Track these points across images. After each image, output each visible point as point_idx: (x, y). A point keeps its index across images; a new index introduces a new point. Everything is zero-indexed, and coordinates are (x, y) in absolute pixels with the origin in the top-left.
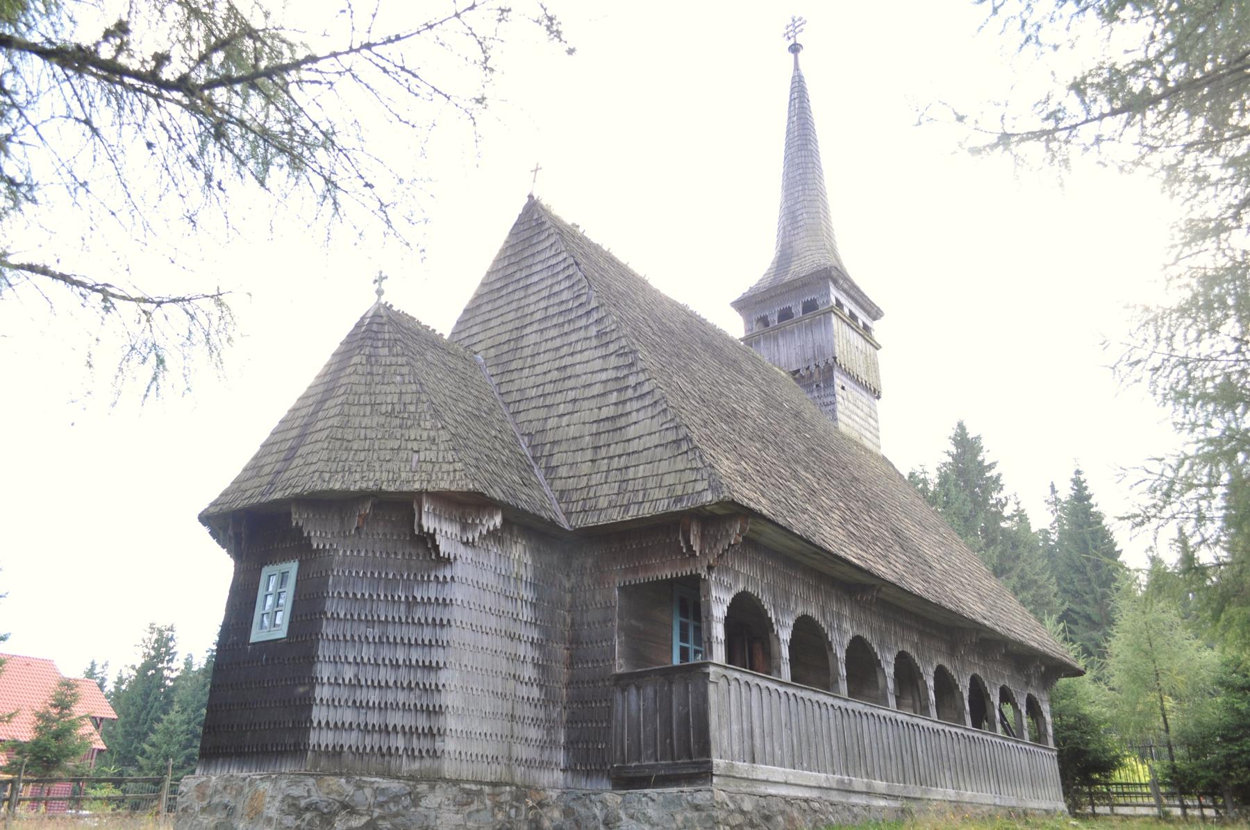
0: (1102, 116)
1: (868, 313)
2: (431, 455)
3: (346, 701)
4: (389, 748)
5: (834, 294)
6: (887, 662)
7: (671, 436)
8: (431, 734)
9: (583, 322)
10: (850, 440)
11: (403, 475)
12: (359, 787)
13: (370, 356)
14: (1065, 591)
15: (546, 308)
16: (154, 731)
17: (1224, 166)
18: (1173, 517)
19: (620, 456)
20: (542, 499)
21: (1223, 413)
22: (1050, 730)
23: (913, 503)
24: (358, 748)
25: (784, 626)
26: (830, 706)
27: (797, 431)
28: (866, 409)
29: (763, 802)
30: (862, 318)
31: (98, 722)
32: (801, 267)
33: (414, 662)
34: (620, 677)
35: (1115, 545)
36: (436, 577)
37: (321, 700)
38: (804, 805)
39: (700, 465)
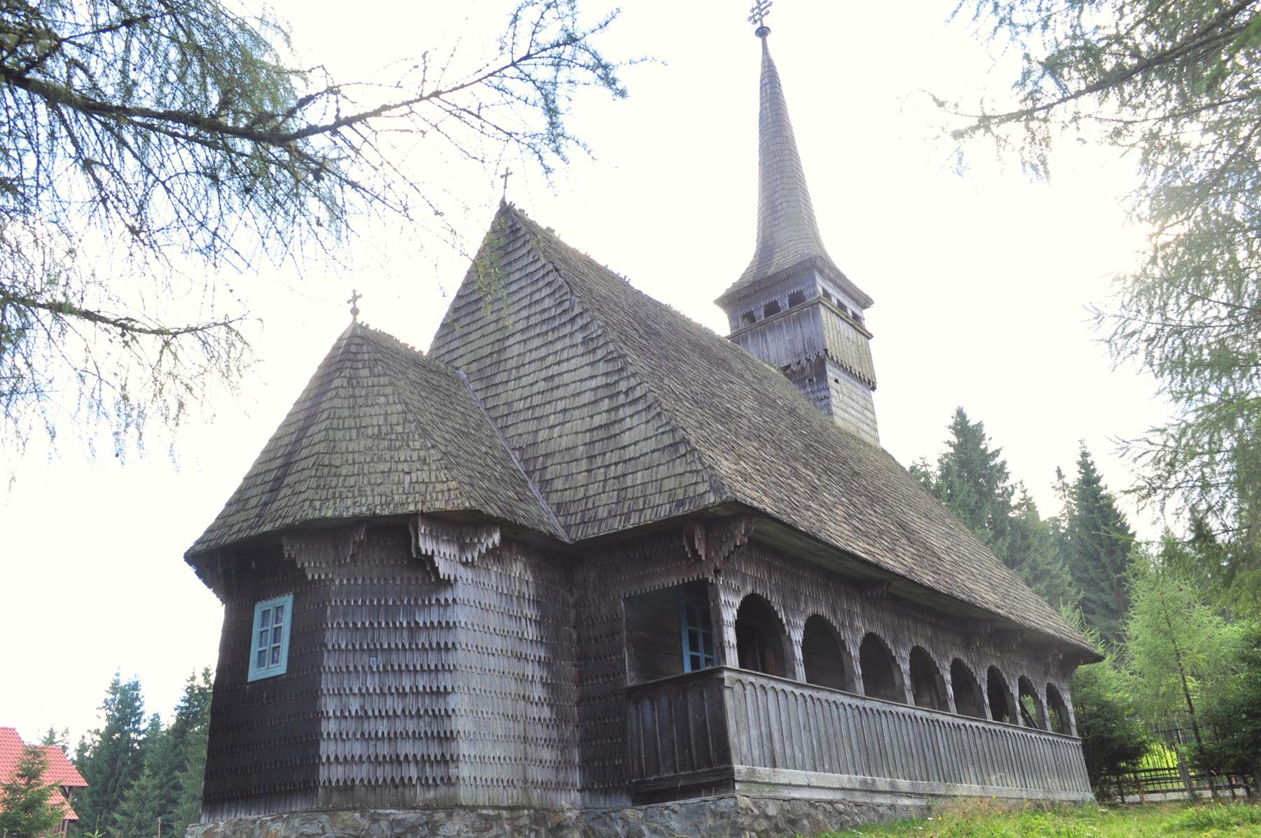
0: (1079, 94)
1: (857, 302)
2: (424, 476)
3: (354, 734)
4: (402, 778)
5: (821, 284)
6: (902, 658)
7: (667, 440)
8: (444, 761)
9: (568, 329)
10: (847, 434)
11: (397, 498)
12: (375, 820)
13: (350, 378)
14: (1079, 580)
15: (528, 318)
16: (124, 799)
17: (1205, 131)
18: (1178, 486)
19: (616, 464)
20: (541, 514)
21: (1219, 379)
22: (1073, 720)
23: (916, 495)
24: (369, 781)
25: (795, 627)
26: (848, 705)
27: (793, 427)
28: (862, 402)
29: (787, 806)
30: (851, 307)
31: (66, 791)
32: (783, 261)
33: (421, 689)
34: (632, 690)
35: (1128, 528)
36: (438, 600)
37: (329, 734)
38: (828, 807)
39: (700, 467)
